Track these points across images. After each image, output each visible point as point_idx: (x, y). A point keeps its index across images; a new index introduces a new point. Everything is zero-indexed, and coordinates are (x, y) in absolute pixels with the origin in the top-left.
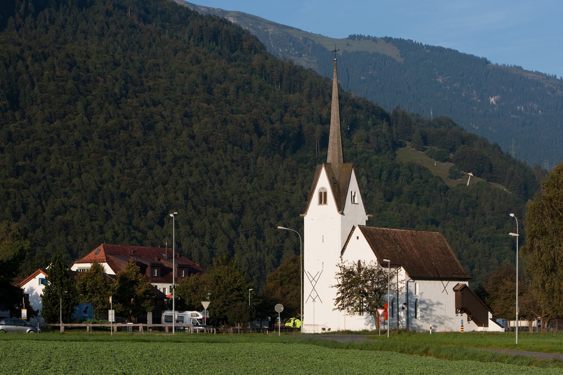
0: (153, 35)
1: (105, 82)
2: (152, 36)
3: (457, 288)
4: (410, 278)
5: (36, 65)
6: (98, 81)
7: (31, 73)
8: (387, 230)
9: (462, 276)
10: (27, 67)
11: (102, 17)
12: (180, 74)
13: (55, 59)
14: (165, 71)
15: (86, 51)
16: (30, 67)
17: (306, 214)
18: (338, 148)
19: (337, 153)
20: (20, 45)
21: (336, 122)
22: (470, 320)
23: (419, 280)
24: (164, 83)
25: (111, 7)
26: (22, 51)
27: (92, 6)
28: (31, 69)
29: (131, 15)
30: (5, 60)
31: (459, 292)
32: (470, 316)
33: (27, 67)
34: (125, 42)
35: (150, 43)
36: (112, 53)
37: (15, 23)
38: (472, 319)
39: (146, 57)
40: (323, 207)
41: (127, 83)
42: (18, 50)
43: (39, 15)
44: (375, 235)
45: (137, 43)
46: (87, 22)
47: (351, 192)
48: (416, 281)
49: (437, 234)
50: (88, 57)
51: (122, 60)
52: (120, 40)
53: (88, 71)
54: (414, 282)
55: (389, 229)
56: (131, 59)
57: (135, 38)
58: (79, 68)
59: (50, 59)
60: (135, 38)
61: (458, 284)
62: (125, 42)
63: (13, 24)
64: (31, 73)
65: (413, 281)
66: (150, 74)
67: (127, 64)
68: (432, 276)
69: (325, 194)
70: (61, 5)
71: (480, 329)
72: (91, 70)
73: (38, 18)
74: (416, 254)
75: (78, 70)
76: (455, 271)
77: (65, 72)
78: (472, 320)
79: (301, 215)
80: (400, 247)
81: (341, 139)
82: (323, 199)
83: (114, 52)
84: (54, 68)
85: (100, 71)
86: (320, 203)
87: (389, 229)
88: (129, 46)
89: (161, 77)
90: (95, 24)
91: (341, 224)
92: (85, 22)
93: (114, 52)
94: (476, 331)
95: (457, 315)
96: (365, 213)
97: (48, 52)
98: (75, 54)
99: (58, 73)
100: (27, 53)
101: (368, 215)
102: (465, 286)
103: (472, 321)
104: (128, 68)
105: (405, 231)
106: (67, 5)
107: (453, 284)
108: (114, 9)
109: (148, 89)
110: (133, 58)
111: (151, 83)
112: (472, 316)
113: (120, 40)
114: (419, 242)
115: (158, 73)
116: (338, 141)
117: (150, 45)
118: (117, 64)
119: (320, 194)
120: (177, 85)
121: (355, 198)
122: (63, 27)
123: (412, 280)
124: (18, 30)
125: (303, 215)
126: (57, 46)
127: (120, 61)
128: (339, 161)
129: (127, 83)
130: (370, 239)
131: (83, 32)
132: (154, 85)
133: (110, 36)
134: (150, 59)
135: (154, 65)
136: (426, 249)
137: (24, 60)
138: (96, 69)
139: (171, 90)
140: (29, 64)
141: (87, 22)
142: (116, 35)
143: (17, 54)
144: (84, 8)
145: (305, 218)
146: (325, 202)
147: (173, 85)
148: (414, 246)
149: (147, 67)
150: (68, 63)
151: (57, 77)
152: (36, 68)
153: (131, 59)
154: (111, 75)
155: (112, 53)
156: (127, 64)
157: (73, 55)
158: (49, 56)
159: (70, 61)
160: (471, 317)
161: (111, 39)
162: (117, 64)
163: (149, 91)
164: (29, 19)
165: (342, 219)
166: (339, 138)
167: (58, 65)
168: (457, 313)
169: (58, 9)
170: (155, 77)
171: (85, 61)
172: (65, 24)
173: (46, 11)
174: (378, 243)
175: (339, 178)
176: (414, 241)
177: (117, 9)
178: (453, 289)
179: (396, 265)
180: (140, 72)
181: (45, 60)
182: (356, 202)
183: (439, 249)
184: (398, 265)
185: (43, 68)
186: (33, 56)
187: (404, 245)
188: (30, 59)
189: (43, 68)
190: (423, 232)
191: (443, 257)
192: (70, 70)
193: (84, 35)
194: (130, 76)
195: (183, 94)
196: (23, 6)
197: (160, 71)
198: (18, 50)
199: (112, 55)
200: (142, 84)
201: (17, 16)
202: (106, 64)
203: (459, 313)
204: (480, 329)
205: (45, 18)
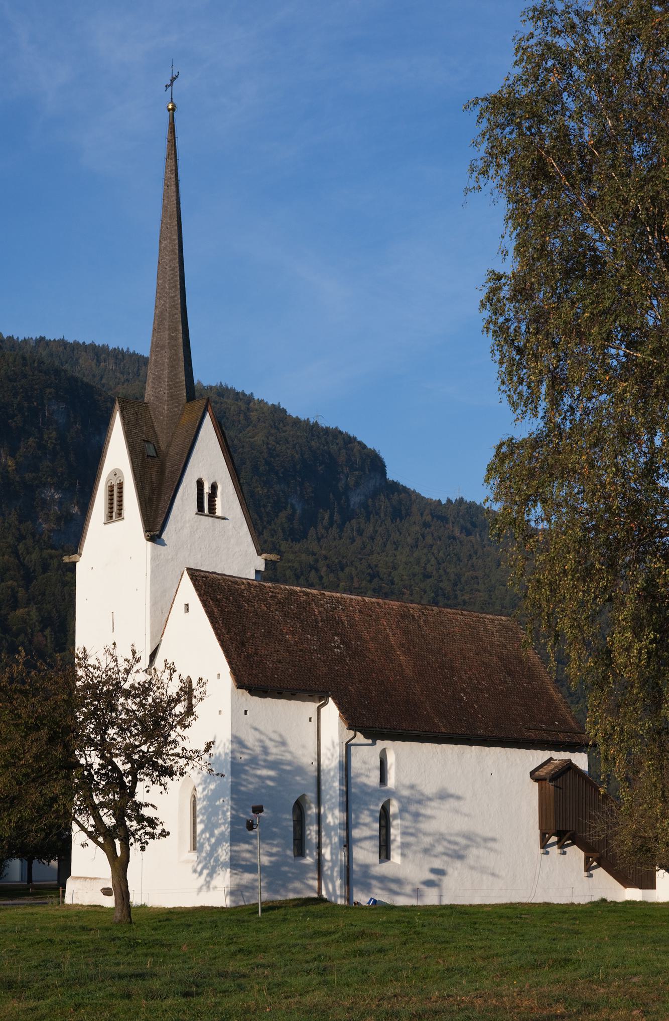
0: (475, 546)
1: (411, 595)
2: (473, 547)
3: (542, 773)
4: (352, 733)
5: (332, 575)
6: (403, 594)
7: (325, 584)
8: (307, 594)
9: (561, 737)
10: (321, 578)
11: (417, 528)
12: (501, 587)
13: (353, 569)
14: (485, 584)
15: (393, 562)
16: (325, 577)
17: (80, 555)
18: (170, 358)
19: (166, 372)
20: (314, 554)
21: (167, 286)
22: (595, 867)
23: (393, 740)
24: (481, 597)
25: (428, 518)
26: (317, 561)
27: (408, 517)
28: (325, 580)
29: (453, 527)
30: (296, 570)
31: (550, 786)
32: (590, 855)
33: (321, 578)
34: (441, 554)
35: (470, 555)
36: (423, 565)
37: (317, 533)
38: (600, 865)
39: (464, 569)
40: (116, 525)
41: (437, 596)
42: (311, 559)
43: (346, 526)
44: (248, 601)
45: (455, 555)
46: (400, 534)
47: (200, 484)
48: (381, 744)
49: (502, 620)
50: (395, 568)
51: (434, 572)
52: (435, 552)
53: (393, 583)
54: (374, 744)
55: (315, 592)
56: (445, 571)
57: (453, 550)
58: (382, 579)
59: (347, 570)
60: (453, 550)
61: (551, 759)
62: (441, 554)
63: (315, 535)
64: (325, 584)
65: (370, 741)
66: (465, 587)
67: (440, 576)
68: (443, 730)
69: (121, 486)
70: (372, 516)
71: (634, 894)
72: (396, 582)
73: (345, 529)
74: (400, 665)
75: (380, 582)
76: (542, 722)
77: (364, 583)
78: (599, 865)
79: (66, 559)
80: (343, 642)
81: (181, 335)
82: (115, 511)
83: (426, 564)
84: (352, 578)
85: (407, 582)
86: (110, 518)
87: (315, 592)
88: (446, 559)
89: (479, 591)
90: (409, 535)
91: (152, 572)
92: (398, 533)
93: (426, 564)
94: (609, 900)
95: (547, 853)
96: (252, 549)
97: (346, 562)
98: (379, 565)
99: (356, 585)
100: (321, 564)
101: (264, 556)
102: (569, 766)
103: (601, 869)
104: (441, 581)
105: (380, 601)
106: (380, 517)
107: (537, 757)
108: (432, 520)
109: (462, 603)
110: (448, 570)
111: (466, 597)
112: (597, 855)
113: (435, 552)
114: (423, 636)
115: (475, 586)
116: (171, 338)
117: (470, 557)
118: (427, 576)
119: (111, 489)
120: (497, 599)
121: (218, 501)
122: (372, 538)
123: (366, 737)
124: (319, 542)
125: (73, 558)
126: (360, 556)
127: (432, 573)
128: (172, 396)
129: (437, 596)
130: (222, 611)
131: (395, 543)
132: (470, 599)
133: (425, 547)
134: (469, 571)
135: (472, 578)
136: (445, 655)
137: (317, 570)
138: (402, 580)
139: (489, 604)
140: (323, 574)
141: (400, 534)
142: (431, 546)
143: (310, 564)
144: (398, 519)
145: (78, 566)
146: (120, 514)
147: (492, 599)
148: (403, 645)
149: (463, 580)
150: (369, 574)
151: (355, 588)
152: (331, 579)
153: (445, 571)
154: (419, 587)
155: (423, 565)
156: (440, 576)
157: (376, 566)
158: (347, 566)
159: (371, 572)
160: (594, 858)
161: (425, 550)
162: (427, 576)
163: (464, 605)
164: (334, 530)
165: (154, 559)
166: (176, 330)
167: (356, 576)
168: (544, 845)
169: (368, 519)
170: (472, 590)
171: (391, 573)
172: (375, 535)
173: (354, 522)
174: (254, 624)
175: (169, 445)
176: (406, 632)
177: (435, 520)
178: (532, 774)
179: (305, 691)
180: (455, 585)
181: (342, 570)
182: (219, 512)
183: (495, 659)
184: (311, 691)
185: (338, 579)
186: (328, 566)
187: (359, 638)
188: (324, 569)
189: (338, 579)
190: (449, 610)
191: (505, 682)
192: (370, 581)
193: (394, 546)
194: (441, 589)
195: (503, 607)
196: (327, 517)
197: (478, 584)
198: (311, 559)
199: (424, 567)
200: (456, 597)
201: (320, 526)
202: (414, 575)
203: (553, 844)
204: (634, 894)
205: (353, 529)
